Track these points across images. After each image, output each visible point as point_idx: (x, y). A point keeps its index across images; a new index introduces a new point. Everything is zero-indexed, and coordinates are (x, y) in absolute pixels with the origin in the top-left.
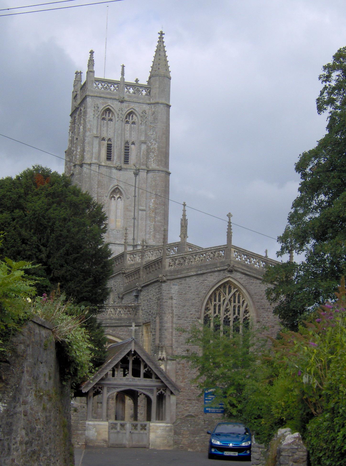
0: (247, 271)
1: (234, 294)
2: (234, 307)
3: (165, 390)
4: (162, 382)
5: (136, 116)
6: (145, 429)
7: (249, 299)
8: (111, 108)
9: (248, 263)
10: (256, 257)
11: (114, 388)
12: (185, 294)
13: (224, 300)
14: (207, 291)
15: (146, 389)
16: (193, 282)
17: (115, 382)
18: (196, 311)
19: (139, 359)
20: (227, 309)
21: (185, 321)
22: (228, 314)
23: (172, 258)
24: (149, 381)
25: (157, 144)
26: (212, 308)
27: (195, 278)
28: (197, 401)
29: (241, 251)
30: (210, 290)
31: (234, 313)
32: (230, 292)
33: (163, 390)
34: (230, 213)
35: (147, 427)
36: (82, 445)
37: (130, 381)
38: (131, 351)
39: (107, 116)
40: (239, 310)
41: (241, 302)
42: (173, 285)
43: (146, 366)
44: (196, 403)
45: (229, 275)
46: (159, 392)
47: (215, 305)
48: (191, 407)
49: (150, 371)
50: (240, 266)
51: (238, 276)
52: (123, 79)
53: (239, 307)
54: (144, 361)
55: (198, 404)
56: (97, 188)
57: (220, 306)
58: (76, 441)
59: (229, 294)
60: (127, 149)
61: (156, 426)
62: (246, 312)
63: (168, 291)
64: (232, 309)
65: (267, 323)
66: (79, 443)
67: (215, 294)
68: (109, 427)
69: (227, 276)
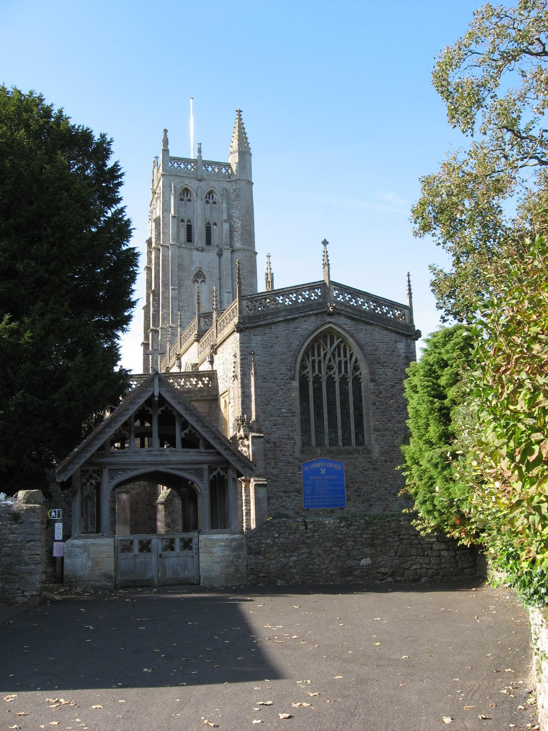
0: (354, 314)
1: (338, 346)
2: (340, 362)
3: (225, 470)
4: (219, 454)
5: (216, 194)
6: (191, 548)
7: (359, 350)
8: (188, 187)
9: (353, 304)
10: (364, 296)
11: (123, 470)
12: (271, 347)
13: (325, 355)
14: (301, 342)
15: (188, 469)
16: (280, 330)
17: (125, 459)
18: (287, 369)
19: (171, 411)
20: (330, 366)
21: (274, 384)
22: (332, 373)
23: (250, 300)
24: (192, 454)
25: (240, 222)
26: (309, 365)
27: (282, 325)
28: (297, 494)
29: (343, 289)
30: (305, 341)
31: (340, 372)
32: (332, 343)
33: (222, 469)
34: (325, 240)
35: (193, 544)
36: (32, 596)
37: (155, 456)
38: (153, 395)
39: (185, 196)
40: (346, 368)
41: (348, 355)
42: (254, 335)
43: (185, 424)
44: (296, 496)
45: (329, 320)
46: (215, 473)
47: (313, 361)
48: (289, 501)
49: (195, 434)
50: (343, 308)
51: (342, 320)
52: (200, 156)
53: (346, 363)
54: (181, 416)
55: (298, 497)
56: (178, 271)
57: (320, 362)
58: (18, 589)
59: (331, 346)
60: (208, 230)
61: (212, 540)
62: (356, 368)
63: (248, 343)
64: (336, 367)
65: (384, 382)
66: (26, 593)
67: (313, 347)
68: (115, 548)
69: (327, 321)
